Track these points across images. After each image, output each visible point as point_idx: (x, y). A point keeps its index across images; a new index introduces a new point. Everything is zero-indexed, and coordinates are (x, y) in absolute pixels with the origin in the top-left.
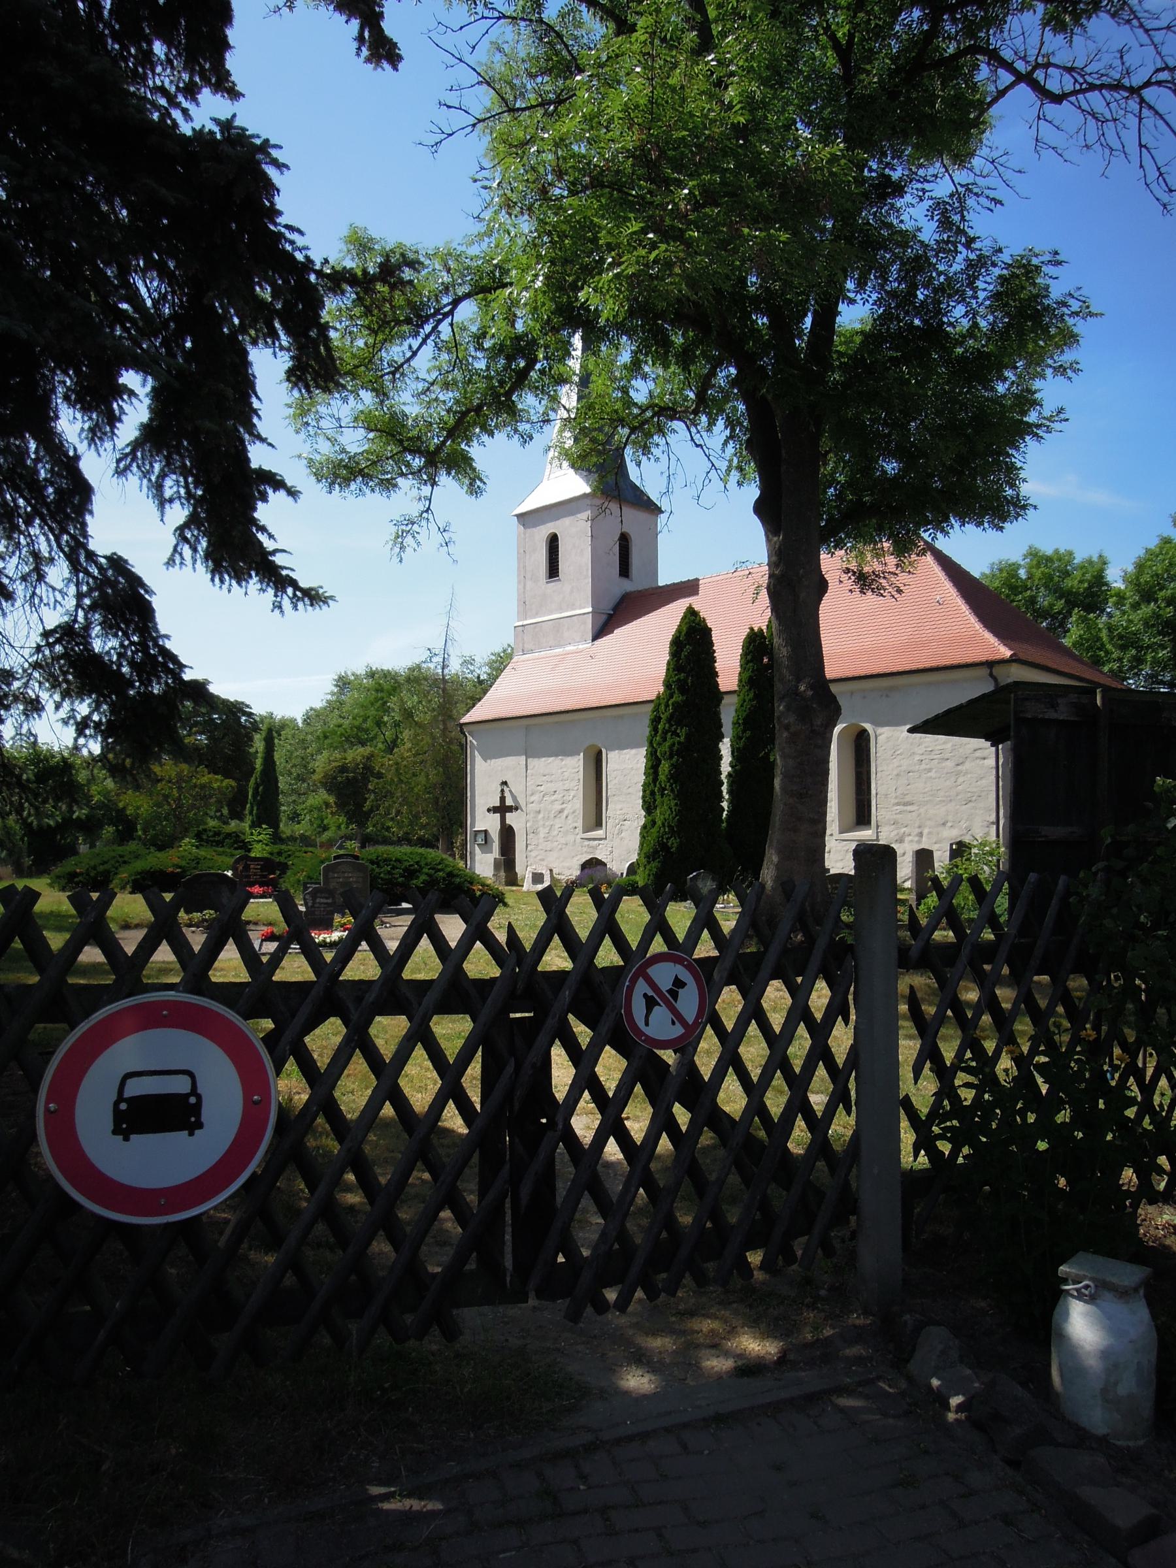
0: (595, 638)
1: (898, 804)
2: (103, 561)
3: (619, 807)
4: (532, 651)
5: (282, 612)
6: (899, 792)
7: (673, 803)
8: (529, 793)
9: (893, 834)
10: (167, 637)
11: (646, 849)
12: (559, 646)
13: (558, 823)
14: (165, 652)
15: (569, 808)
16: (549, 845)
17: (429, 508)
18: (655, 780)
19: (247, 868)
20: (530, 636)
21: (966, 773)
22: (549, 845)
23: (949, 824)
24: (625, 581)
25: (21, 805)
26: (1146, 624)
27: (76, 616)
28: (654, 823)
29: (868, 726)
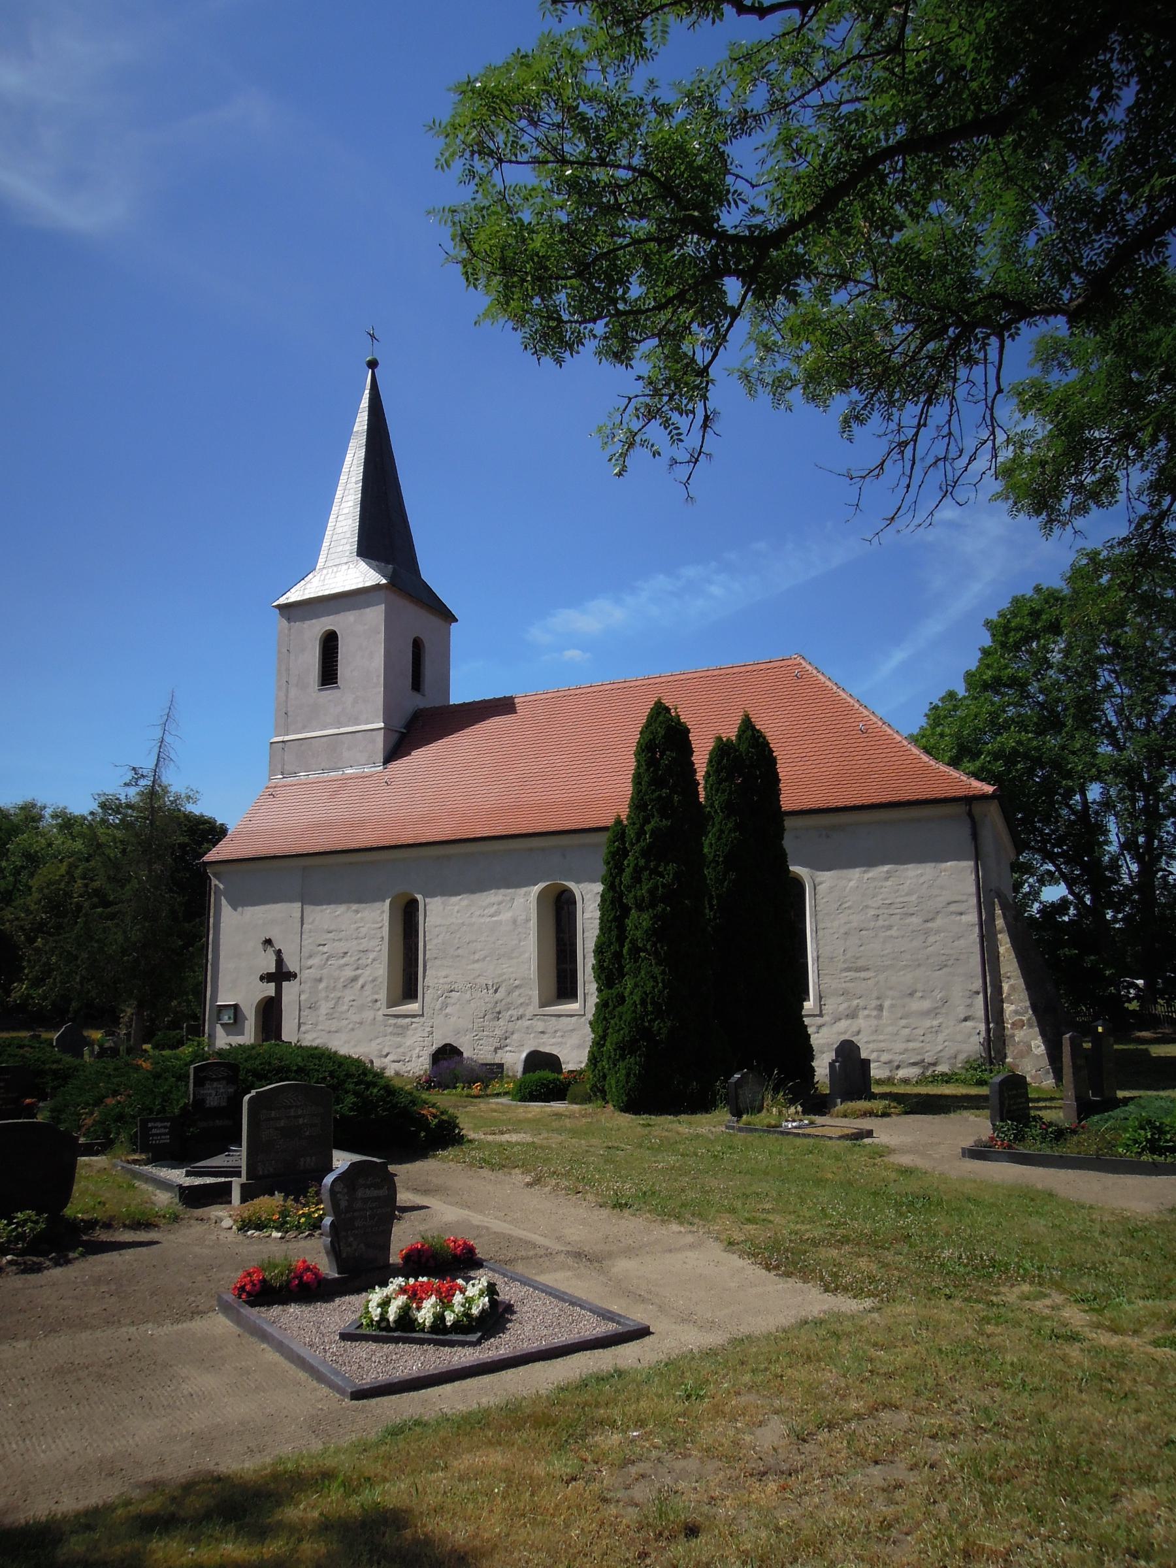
0: (387, 760)
1: (848, 969)
4: (294, 774)
6: (849, 955)
13: (349, 995)
15: (366, 975)
16: (334, 1025)
18: (621, 939)
21: (938, 932)
22: (334, 1025)
23: (919, 994)
24: (418, 696)
28: (621, 999)
29: (572, 885)
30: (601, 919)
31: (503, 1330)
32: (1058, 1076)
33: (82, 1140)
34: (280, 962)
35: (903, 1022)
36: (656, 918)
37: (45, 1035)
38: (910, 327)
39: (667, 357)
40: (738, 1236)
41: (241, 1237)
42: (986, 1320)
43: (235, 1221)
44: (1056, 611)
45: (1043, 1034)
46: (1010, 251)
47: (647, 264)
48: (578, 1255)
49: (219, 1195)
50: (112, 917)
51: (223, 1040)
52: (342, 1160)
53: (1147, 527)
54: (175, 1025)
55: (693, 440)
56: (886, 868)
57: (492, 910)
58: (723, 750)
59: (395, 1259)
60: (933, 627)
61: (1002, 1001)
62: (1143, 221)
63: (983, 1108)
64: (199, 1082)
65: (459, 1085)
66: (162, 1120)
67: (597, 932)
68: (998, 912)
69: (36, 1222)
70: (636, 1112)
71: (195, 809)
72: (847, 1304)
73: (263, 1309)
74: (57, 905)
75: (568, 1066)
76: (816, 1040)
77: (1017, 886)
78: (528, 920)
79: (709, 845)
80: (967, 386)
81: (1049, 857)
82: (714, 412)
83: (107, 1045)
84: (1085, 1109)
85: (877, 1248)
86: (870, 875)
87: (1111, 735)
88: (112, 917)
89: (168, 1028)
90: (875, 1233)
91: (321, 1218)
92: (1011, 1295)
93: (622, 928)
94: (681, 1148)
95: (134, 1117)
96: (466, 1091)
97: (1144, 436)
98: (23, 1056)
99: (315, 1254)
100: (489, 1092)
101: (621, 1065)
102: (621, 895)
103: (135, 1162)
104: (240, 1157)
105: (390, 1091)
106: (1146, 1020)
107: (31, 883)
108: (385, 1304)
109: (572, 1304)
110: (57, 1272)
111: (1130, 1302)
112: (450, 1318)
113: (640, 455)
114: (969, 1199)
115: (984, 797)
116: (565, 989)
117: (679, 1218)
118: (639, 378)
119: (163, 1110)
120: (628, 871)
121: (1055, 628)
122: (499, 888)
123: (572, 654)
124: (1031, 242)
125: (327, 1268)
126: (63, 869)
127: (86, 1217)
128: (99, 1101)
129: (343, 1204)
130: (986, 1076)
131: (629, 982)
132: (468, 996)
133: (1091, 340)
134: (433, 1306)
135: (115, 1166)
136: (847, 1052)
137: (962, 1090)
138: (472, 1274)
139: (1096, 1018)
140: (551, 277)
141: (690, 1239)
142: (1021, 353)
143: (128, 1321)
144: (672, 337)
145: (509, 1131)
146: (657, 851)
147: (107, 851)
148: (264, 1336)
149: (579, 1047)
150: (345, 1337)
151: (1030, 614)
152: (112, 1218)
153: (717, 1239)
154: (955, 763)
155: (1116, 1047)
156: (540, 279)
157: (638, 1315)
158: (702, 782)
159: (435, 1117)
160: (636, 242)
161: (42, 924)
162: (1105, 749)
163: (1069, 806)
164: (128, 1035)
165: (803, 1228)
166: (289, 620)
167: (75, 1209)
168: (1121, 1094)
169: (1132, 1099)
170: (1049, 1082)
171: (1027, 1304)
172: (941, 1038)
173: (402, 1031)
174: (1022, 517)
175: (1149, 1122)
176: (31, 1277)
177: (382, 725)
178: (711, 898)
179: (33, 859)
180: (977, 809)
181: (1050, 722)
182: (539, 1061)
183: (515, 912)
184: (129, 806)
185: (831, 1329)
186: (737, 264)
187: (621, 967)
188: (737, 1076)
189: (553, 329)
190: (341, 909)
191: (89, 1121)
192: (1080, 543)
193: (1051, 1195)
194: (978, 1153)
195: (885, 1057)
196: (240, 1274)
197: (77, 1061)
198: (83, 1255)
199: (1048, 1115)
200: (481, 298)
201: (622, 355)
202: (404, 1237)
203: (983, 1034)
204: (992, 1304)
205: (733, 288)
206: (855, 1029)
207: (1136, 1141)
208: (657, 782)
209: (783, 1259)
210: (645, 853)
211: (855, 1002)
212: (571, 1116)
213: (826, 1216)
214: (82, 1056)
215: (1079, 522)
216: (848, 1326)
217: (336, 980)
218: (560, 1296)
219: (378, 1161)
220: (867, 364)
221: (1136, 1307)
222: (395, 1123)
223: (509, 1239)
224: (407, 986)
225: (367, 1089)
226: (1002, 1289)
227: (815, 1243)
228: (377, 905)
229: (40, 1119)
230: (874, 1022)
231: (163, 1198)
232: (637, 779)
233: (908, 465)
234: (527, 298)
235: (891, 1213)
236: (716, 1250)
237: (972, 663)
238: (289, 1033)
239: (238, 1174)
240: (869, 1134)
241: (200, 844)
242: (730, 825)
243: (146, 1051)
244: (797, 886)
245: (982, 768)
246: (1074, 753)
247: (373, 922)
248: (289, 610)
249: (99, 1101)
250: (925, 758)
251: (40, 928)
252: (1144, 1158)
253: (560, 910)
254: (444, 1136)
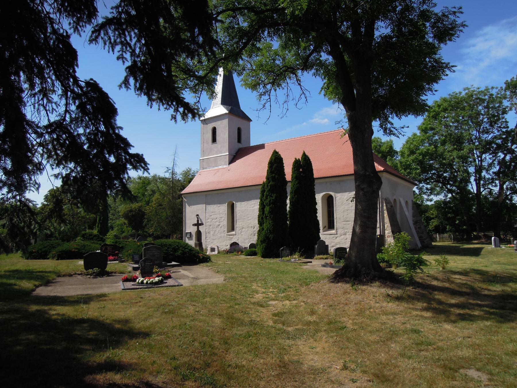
1: (344, 221)
2: (83, 84)
4: (206, 168)
5: (176, 121)
6: (345, 217)
7: (271, 222)
10: (121, 128)
11: (260, 239)
12: (217, 166)
13: (218, 229)
14: (119, 137)
15: (222, 224)
16: (214, 238)
17: (199, 101)
18: (263, 213)
19: (106, 249)
20: (204, 164)
25: (30, 222)
26: (413, 161)
27: (65, 116)
28: (263, 229)
29: (332, 194)
68: (384, 204)
112: (149, 282)
131: (265, 225)
167: (108, 269)
179: (154, 192)
190: (215, 206)
247: (223, 209)
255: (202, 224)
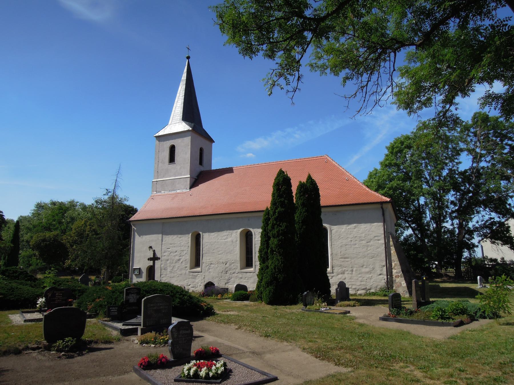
0: (191, 188)
1: (341, 258)
3: (208, 258)
8: (163, 251)
9: (340, 271)
13: (177, 265)
15: (183, 258)
16: (172, 275)
18: (268, 247)
21: (371, 246)
22: (172, 275)
23: (365, 266)
24: (201, 166)
28: (267, 267)
29: (251, 229)
30: (261, 241)
31: (229, 378)
32: (410, 293)
33: (88, 313)
34: (154, 254)
35: (360, 275)
36: (279, 240)
37: (76, 278)
38: (366, 49)
39: (286, 57)
40: (306, 347)
41: (141, 346)
42: (389, 375)
43: (139, 341)
44: (409, 141)
45: (405, 279)
46: (398, 25)
47: (280, 26)
48: (253, 353)
49: (134, 332)
50: (99, 238)
51: (135, 280)
52: (175, 321)
53: (441, 115)
54: (119, 275)
55: (294, 84)
56: (355, 225)
57: (225, 238)
58: (302, 186)
59: (193, 354)
60: (367, 148)
61: (392, 269)
62: (441, 16)
63: (386, 304)
64: (127, 294)
65: (214, 295)
66: (115, 307)
67: (259, 245)
68: (391, 240)
69: (72, 341)
70: (272, 305)
71: (127, 203)
72: (343, 370)
73: (148, 371)
74: (81, 234)
75: (249, 289)
76: (331, 281)
77: (397, 231)
78: (236, 241)
79: (297, 217)
80: (384, 69)
81: (407, 222)
82: (301, 75)
83: (96, 281)
84: (420, 304)
85: (352, 351)
86: (349, 227)
87: (427, 183)
88: (99, 238)
89: (117, 276)
90: (352, 345)
91: (168, 340)
92: (397, 366)
93: (268, 244)
94: (287, 317)
95: (105, 306)
96: (216, 297)
97: (441, 85)
98: (68, 285)
99: (165, 352)
100: (223, 297)
101: (267, 289)
102: (268, 233)
103: (106, 321)
104: (140, 319)
105: (191, 297)
106: (438, 275)
107: (72, 227)
108: (189, 369)
109: (252, 369)
110: (79, 358)
111: (436, 369)
112: (211, 374)
113: (276, 89)
114: (382, 334)
115: (386, 202)
116: (249, 263)
117: (287, 341)
118: (277, 63)
119: (115, 303)
120: (270, 225)
121: (409, 147)
122: (227, 230)
123: (250, 155)
124: (405, 22)
125: (169, 357)
126: (83, 222)
127: (89, 339)
128: (94, 300)
129: (175, 336)
130: (387, 293)
131: (270, 262)
132: (217, 266)
133: (424, 54)
134: (205, 370)
135: (99, 322)
136: (342, 285)
137: (379, 298)
138: (218, 359)
139: (422, 275)
140: (249, 30)
141: (290, 347)
142: (402, 57)
143: (103, 375)
144: (288, 51)
145: (230, 311)
146: (280, 218)
147: (98, 217)
148: (149, 380)
149: (253, 283)
150: (176, 380)
151: (400, 143)
152: (98, 340)
153: (299, 347)
154: (377, 190)
155: (430, 284)
156: (245, 30)
157: (274, 373)
158: (295, 196)
159: (206, 306)
160: (277, 19)
161: (76, 241)
162: (425, 186)
163: (414, 205)
164: (104, 278)
165: (328, 344)
166: (159, 141)
167: (86, 336)
168: (431, 300)
169: (435, 301)
170: (407, 295)
171: (402, 370)
172: (372, 280)
173: (195, 277)
174: (401, 110)
175: (441, 309)
176: (71, 360)
177: (189, 176)
178: (297, 234)
179: (73, 219)
180: (384, 206)
181: (407, 178)
182: (240, 288)
183: (232, 238)
184: (105, 202)
185: (337, 378)
186: (310, 27)
187: (268, 257)
188: (306, 293)
189: (249, 47)
190: (175, 236)
191: (90, 307)
192: (419, 119)
193: (409, 333)
194: (385, 319)
195: (354, 287)
196: (141, 359)
197: (86, 287)
198: (88, 352)
199: (408, 306)
200: (226, 37)
201: (271, 55)
202: (196, 346)
203: (386, 279)
204: (390, 370)
205: (308, 35)
206: (344, 278)
207: (436, 315)
208: (280, 196)
209: (322, 354)
210: (276, 219)
211: (344, 269)
212: (251, 306)
213: (335, 340)
214: (88, 285)
215: (419, 112)
216: (343, 377)
217: (173, 260)
218: (247, 367)
219: (186, 321)
220: (351, 61)
221: (438, 371)
222: (192, 308)
223: (230, 347)
224: (197, 262)
225: (183, 296)
226: (394, 365)
227: (332, 349)
228: (187, 235)
229: (74, 306)
230: (350, 275)
231: (115, 333)
232: (273, 195)
233: (364, 94)
234: (240, 37)
235: (357, 339)
236: (299, 351)
237: (382, 158)
238: (157, 278)
239: (140, 325)
240: (349, 312)
241: (128, 215)
242: (304, 210)
243: (110, 283)
244: (325, 230)
245: (386, 193)
246: (415, 188)
247: (185, 241)
248: (159, 138)
249: (94, 300)
250: (367, 189)
251: (75, 242)
252: (439, 321)
253: (247, 237)
254: (209, 312)
255: (158, 259)
